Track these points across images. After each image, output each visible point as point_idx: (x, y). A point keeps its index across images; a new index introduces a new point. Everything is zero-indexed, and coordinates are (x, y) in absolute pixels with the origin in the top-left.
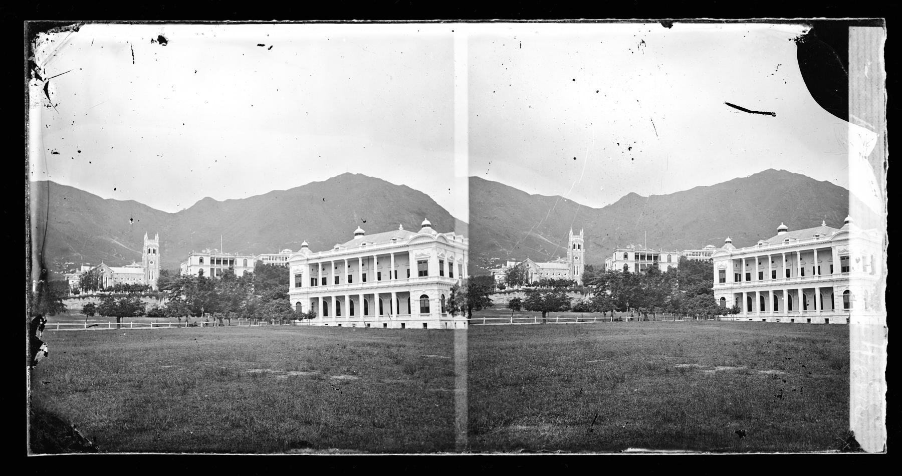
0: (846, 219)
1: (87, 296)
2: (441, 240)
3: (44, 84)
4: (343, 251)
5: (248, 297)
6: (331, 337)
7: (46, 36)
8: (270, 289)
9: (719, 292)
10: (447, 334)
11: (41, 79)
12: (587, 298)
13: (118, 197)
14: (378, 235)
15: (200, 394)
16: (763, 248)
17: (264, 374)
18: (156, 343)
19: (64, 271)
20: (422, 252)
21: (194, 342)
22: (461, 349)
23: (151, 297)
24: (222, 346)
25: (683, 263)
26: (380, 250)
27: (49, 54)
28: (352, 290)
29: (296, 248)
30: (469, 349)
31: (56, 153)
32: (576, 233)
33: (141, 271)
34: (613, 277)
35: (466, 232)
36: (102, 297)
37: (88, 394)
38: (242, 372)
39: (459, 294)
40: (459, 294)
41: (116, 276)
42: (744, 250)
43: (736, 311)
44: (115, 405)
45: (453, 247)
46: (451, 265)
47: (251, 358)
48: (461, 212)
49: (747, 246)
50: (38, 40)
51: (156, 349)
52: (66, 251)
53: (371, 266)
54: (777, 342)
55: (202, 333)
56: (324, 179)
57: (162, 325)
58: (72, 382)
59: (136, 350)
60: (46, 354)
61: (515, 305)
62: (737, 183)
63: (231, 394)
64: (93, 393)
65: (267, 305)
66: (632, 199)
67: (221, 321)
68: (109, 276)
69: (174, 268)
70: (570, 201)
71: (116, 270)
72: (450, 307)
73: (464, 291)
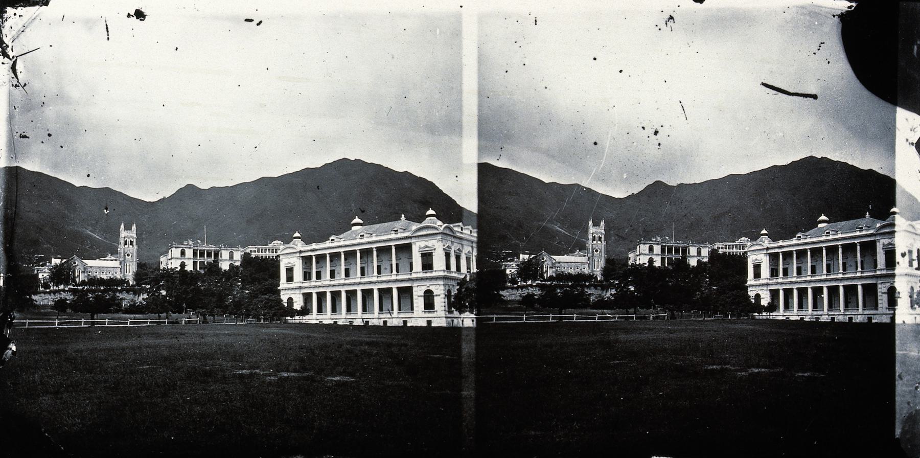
0: (892, 210)
1: (526, 287)
2: (448, 232)
3: (11, 62)
4: (338, 243)
5: (235, 293)
6: (325, 335)
7: (14, 11)
8: (260, 283)
9: (287, 292)
10: (452, 333)
11: (8, 56)
12: (608, 294)
13: (92, 184)
14: (377, 226)
15: (182, 397)
16: (802, 241)
17: (251, 375)
18: (133, 342)
19: (501, 259)
20: (426, 243)
21: (174, 341)
22: (468, 348)
23: (128, 292)
24: (206, 344)
25: (246, 258)
26: (380, 241)
27: (17, 30)
28: (334, 286)
29: (287, 240)
30: (477, 349)
31: (25, 137)
32: (596, 224)
33: (117, 264)
34: (168, 275)
35: (475, 221)
36: (73, 292)
37: (59, 396)
38: (227, 373)
39: (467, 289)
40: (467, 289)
41: (89, 269)
42: (314, 246)
43: (773, 307)
44: (89, 408)
45: (461, 239)
46: (458, 258)
47: (237, 358)
48: (470, 203)
49: (784, 239)
50: (5, 16)
51: (133, 348)
52: (35, 243)
53: (370, 259)
54: (348, 346)
55: (183, 331)
56: (319, 164)
57: (140, 323)
58: (42, 383)
59: (113, 349)
60: (13, 353)
61: (60, 306)
62: (775, 170)
63: (215, 396)
64: (65, 396)
65: (255, 301)
66: (657, 189)
67: (205, 318)
68: (82, 269)
69: (153, 261)
70: (589, 190)
71: (90, 263)
72: (456, 303)
73: (473, 285)
